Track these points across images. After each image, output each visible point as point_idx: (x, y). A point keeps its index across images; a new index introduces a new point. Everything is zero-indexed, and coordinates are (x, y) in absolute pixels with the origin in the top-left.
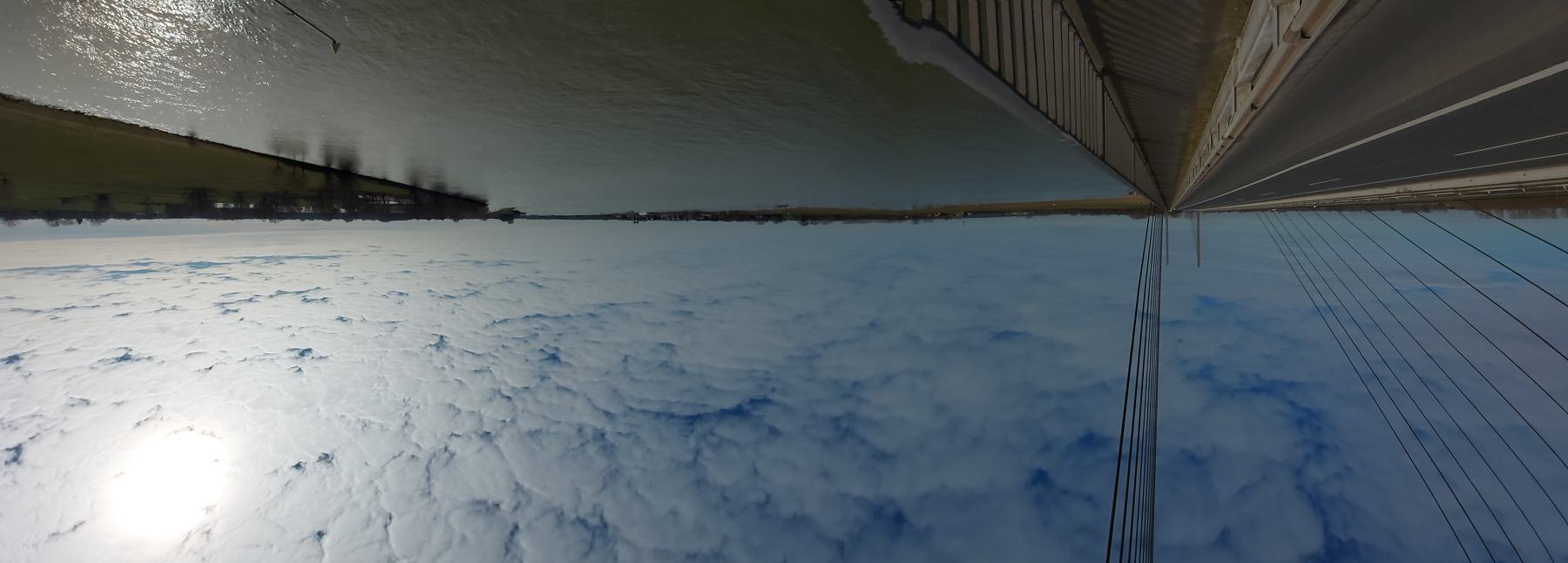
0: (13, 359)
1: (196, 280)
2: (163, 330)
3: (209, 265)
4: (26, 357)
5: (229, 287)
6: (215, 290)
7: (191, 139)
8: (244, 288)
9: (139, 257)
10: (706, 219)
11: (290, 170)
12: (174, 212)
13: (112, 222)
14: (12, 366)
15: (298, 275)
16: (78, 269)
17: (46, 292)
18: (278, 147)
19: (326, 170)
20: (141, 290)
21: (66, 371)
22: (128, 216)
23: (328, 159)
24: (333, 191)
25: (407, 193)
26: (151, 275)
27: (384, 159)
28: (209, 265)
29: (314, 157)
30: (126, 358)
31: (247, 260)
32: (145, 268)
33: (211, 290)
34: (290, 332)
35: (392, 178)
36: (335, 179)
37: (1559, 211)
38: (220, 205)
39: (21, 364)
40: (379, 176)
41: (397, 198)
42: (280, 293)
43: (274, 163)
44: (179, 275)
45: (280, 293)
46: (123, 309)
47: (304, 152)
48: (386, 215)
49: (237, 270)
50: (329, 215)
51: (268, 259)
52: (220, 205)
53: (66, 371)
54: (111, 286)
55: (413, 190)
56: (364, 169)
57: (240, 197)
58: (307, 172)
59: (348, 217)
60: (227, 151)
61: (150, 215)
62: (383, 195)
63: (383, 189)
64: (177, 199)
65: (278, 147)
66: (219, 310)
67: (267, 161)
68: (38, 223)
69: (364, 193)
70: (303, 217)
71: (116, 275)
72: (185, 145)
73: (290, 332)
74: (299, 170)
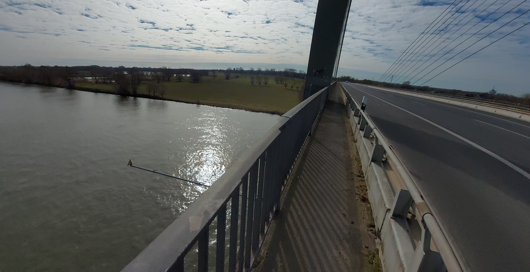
0: (268, 22)
1: (201, 42)
2: (216, 22)
3: (196, 49)
4: (265, 22)
5: (189, 37)
6: (195, 36)
7: (199, 104)
8: (182, 35)
9: (220, 54)
10: (432, 89)
11: (156, 94)
12: (205, 72)
13: (282, 70)
14: (269, 20)
15: (156, 38)
16: (238, 52)
17: (248, 44)
18: (162, 104)
19: (136, 95)
20: (220, 41)
21: (247, 14)
22: (221, 71)
23: (136, 104)
24: (129, 84)
25: (77, 85)
26: (217, 46)
27: (97, 108)
28: (196, 49)
29: (143, 102)
30: (230, 14)
31: (180, 49)
32: (219, 49)
33: (196, 37)
34: (163, 8)
35: (90, 95)
36: (131, 90)
37: (298, 72)
38: (188, 75)
39: (266, 20)
40: (101, 95)
41: (86, 81)
42: (166, 30)
43: (164, 97)
44: (208, 45)
45: (166, 30)
46: (227, 34)
47: (150, 105)
48: (94, 70)
49: (184, 44)
50: (133, 71)
51: (170, 48)
52: (188, 75)
53: (247, 14)
54: (230, 44)
55: (71, 87)
56: (112, 98)
57: (180, 79)
58: (147, 93)
59: (122, 69)
60: (185, 100)
61: (213, 71)
62: (97, 82)
63: (95, 87)
64: (204, 78)
65: (162, 104)
66: (194, 27)
67: (170, 98)
68: (245, 69)
69: (111, 83)
70: (149, 70)
71: (227, 48)
72: (201, 101)
73: (163, 8)
74: (152, 94)
